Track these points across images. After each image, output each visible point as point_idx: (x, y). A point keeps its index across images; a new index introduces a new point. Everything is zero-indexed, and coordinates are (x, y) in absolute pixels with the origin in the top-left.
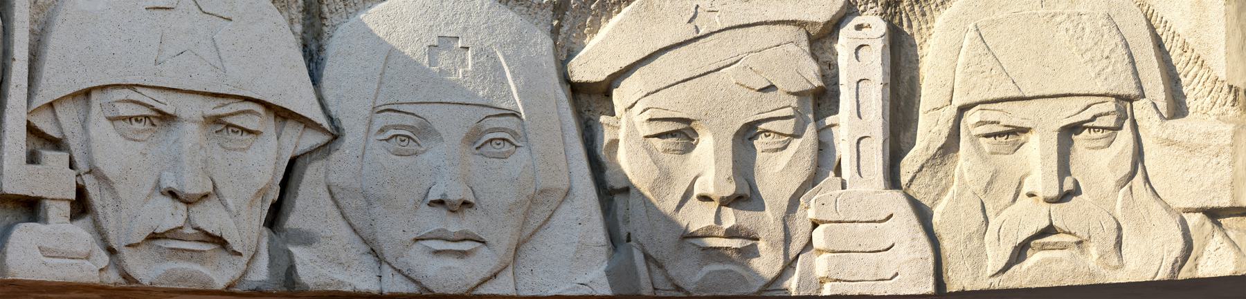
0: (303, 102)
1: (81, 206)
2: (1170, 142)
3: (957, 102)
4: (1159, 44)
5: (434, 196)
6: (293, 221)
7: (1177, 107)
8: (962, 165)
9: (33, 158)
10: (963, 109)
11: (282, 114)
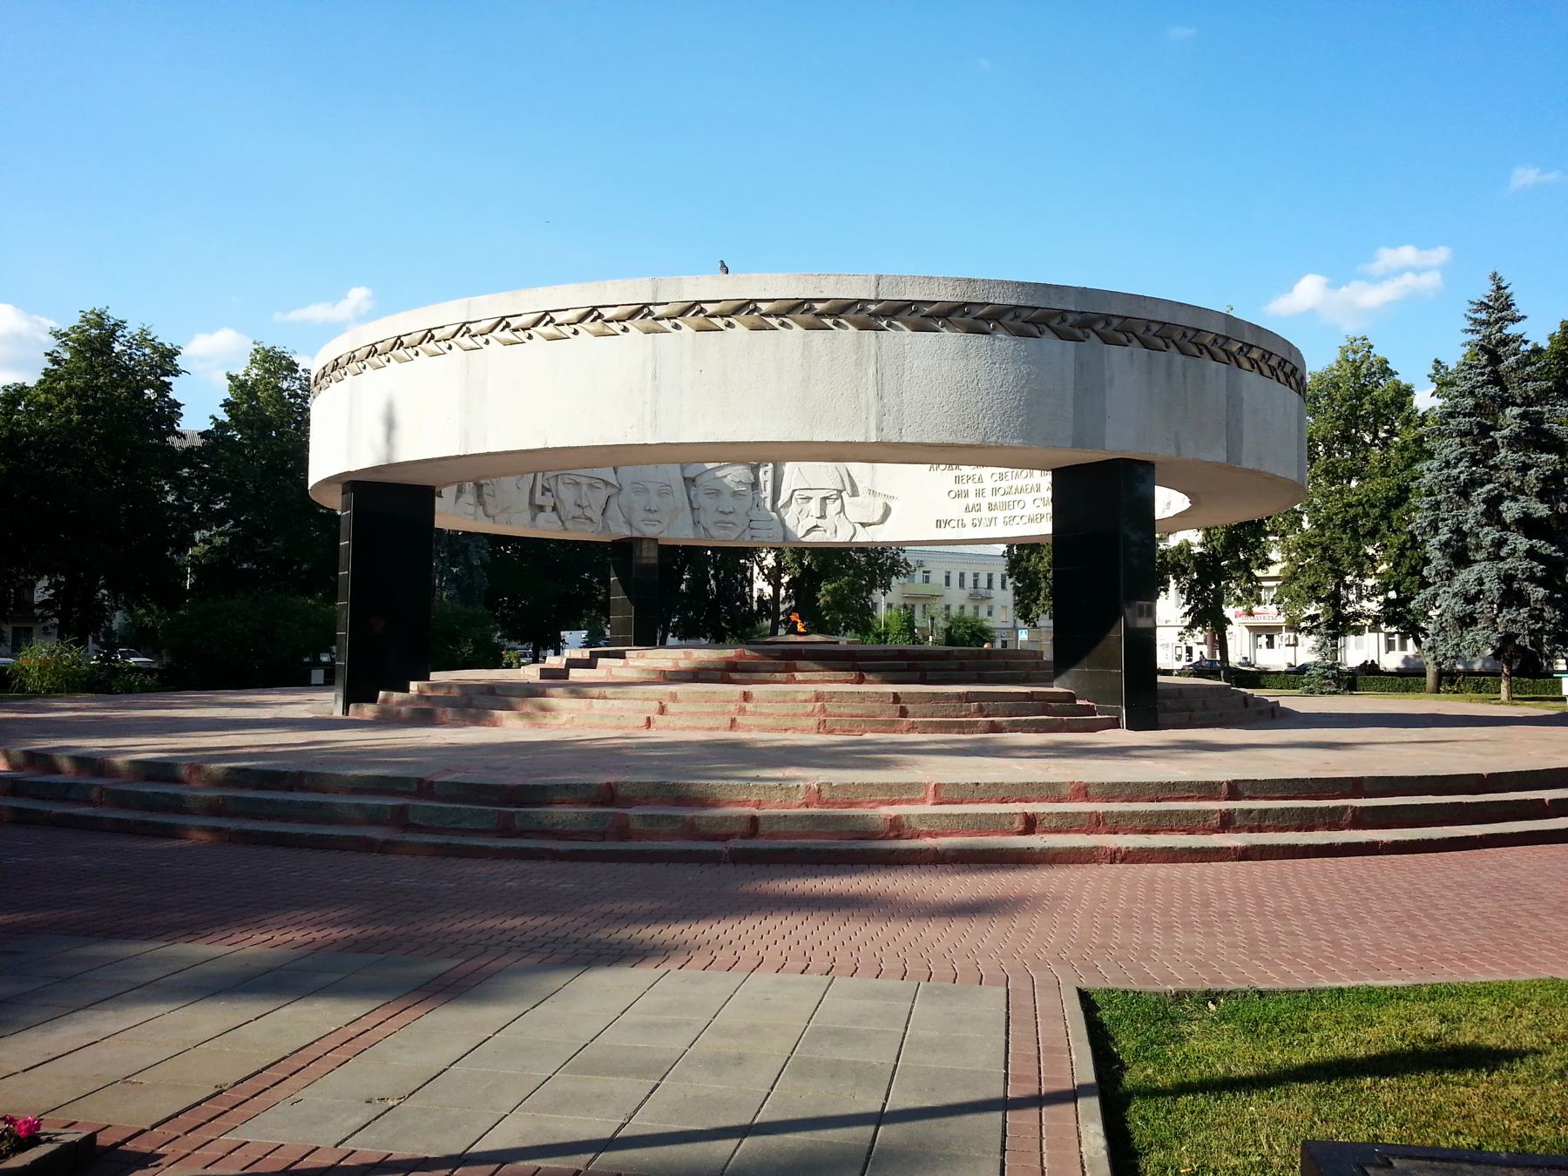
0: (612, 480)
1: (554, 509)
2: (851, 503)
3: (792, 489)
4: (849, 475)
5: (648, 508)
6: (609, 513)
7: (855, 493)
8: (1523, 975)
9: (543, 494)
10: (794, 491)
11: (607, 483)
